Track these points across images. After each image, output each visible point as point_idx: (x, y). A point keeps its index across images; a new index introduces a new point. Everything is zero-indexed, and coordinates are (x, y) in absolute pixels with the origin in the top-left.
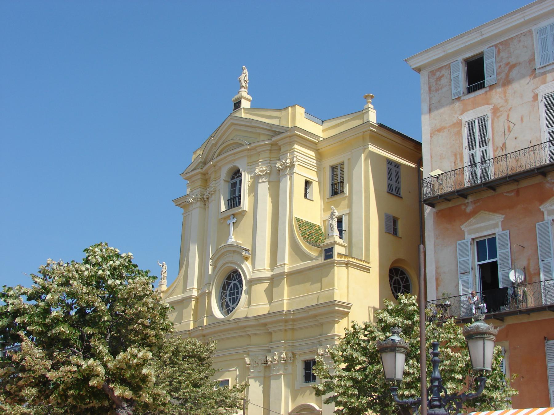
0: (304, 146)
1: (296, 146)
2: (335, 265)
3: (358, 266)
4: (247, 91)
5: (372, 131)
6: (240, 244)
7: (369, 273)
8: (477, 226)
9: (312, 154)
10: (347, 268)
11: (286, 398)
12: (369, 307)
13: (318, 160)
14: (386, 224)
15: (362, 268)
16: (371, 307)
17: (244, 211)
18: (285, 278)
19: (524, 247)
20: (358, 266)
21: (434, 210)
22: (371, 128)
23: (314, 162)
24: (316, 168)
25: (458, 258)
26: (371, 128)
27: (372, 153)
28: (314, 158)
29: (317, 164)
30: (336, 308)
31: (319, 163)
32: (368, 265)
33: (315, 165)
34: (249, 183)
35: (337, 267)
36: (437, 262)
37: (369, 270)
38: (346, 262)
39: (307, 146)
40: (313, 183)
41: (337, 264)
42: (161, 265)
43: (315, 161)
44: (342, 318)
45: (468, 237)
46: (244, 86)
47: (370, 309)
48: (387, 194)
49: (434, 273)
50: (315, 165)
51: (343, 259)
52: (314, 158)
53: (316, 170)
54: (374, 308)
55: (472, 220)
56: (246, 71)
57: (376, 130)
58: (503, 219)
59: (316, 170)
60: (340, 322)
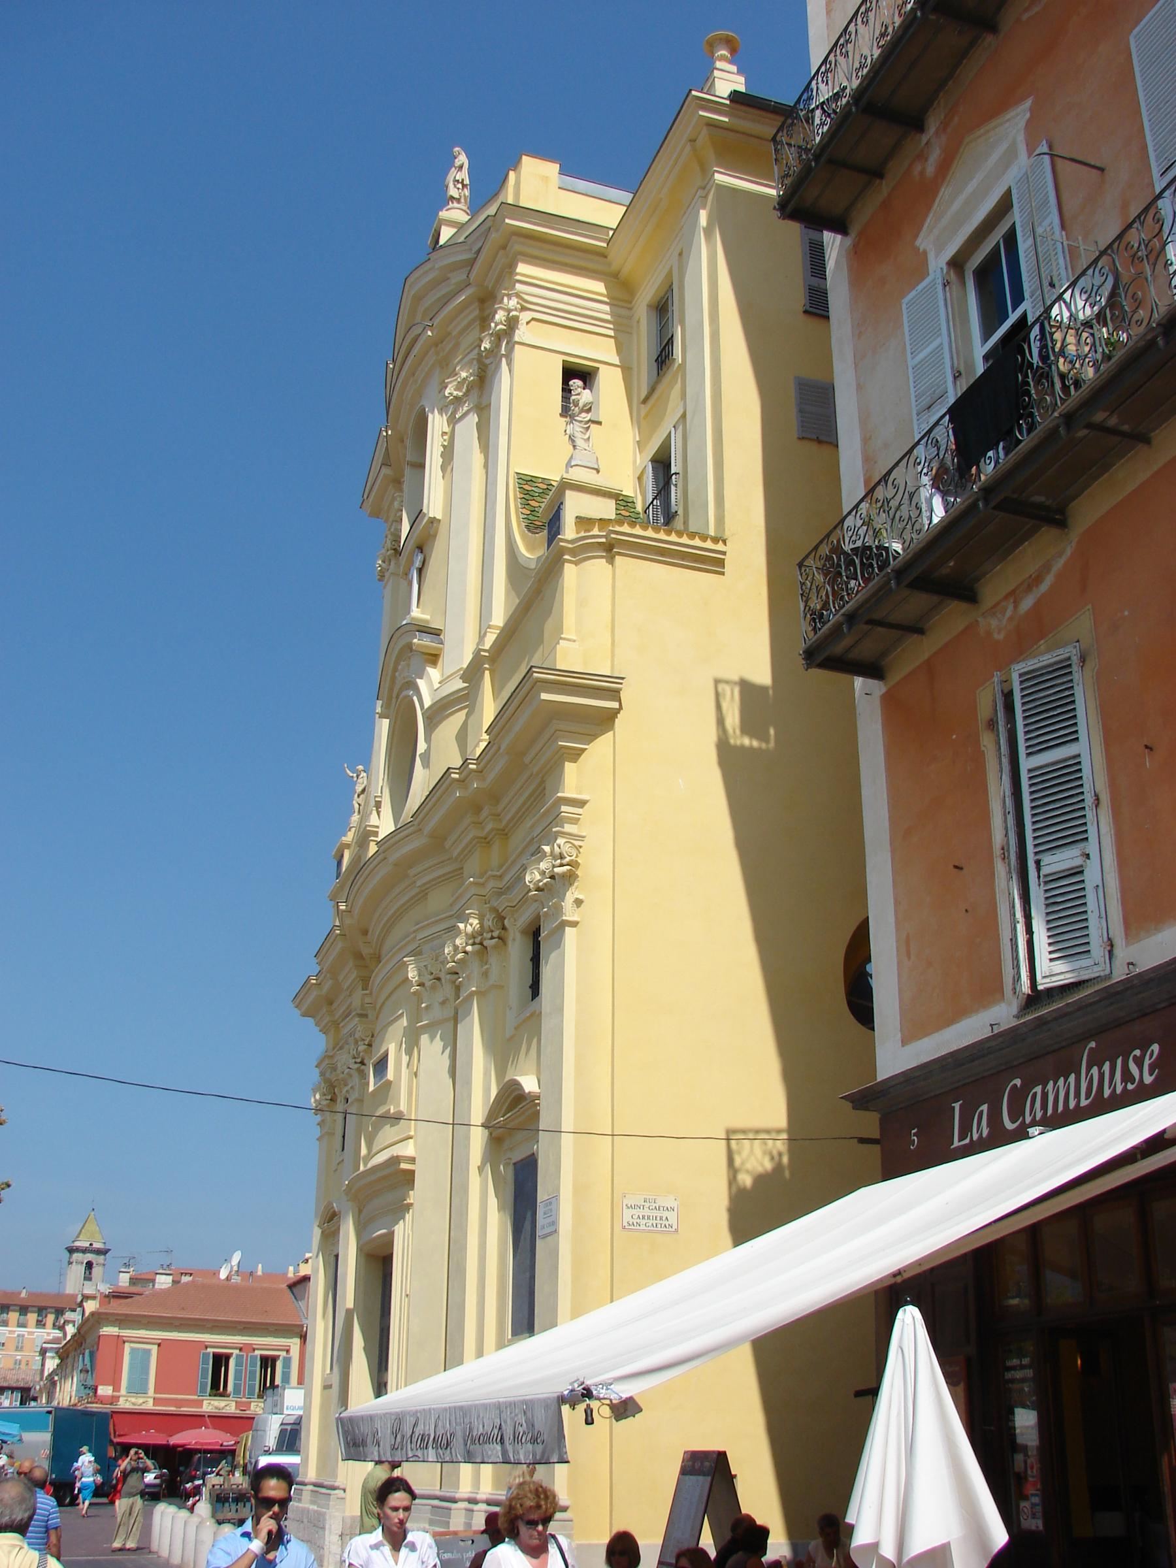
0: (538, 262)
1: (522, 268)
2: (566, 557)
3: (662, 552)
4: (465, 208)
5: (712, 124)
6: (427, 621)
7: (723, 574)
8: (956, 205)
9: (599, 287)
10: (611, 560)
11: (486, 1074)
12: (717, 682)
13: (615, 303)
14: (801, 411)
15: (683, 559)
16: (727, 682)
17: (433, 521)
18: (487, 673)
19: (1102, 170)
20: (662, 552)
21: (848, 241)
22: (701, 113)
23: (604, 311)
24: (611, 326)
25: (909, 356)
26: (701, 113)
27: (722, 189)
28: (606, 299)
29: (612, 314)
30: (544, 696)
31: (624, 312)
32: (720, 547)
33: (608, 317)
34: (445, 437)
35: (576, 563)
36: (864, 418)
37: (721, 563)
38: (603, 540)
39: (566, 265)
40: (601, 371)
41: (573, 552)
42: (355, 775)
43: (607, 308)
44: (592, 737)
45: (938, 263)
46: (457, 196)
47: (726, 689)
48: (802, 317)
49: (859, 463)
50: (608, 317)
51: (595, 532)
52: (606, 299)
53: (611, 333)
54: (746, 686)
55: (945, 192)
56: (462, 159)
57: (727, 120)
58: (1028, 115)
59: (611, 333)
60: (586, 752)
